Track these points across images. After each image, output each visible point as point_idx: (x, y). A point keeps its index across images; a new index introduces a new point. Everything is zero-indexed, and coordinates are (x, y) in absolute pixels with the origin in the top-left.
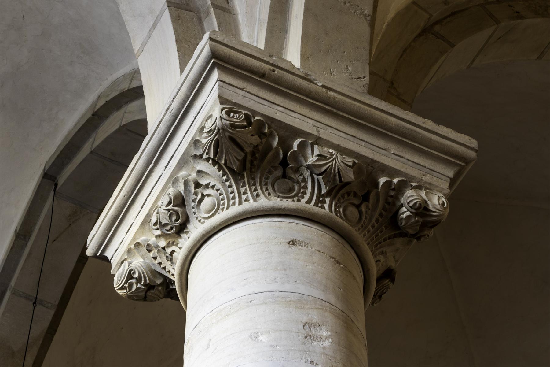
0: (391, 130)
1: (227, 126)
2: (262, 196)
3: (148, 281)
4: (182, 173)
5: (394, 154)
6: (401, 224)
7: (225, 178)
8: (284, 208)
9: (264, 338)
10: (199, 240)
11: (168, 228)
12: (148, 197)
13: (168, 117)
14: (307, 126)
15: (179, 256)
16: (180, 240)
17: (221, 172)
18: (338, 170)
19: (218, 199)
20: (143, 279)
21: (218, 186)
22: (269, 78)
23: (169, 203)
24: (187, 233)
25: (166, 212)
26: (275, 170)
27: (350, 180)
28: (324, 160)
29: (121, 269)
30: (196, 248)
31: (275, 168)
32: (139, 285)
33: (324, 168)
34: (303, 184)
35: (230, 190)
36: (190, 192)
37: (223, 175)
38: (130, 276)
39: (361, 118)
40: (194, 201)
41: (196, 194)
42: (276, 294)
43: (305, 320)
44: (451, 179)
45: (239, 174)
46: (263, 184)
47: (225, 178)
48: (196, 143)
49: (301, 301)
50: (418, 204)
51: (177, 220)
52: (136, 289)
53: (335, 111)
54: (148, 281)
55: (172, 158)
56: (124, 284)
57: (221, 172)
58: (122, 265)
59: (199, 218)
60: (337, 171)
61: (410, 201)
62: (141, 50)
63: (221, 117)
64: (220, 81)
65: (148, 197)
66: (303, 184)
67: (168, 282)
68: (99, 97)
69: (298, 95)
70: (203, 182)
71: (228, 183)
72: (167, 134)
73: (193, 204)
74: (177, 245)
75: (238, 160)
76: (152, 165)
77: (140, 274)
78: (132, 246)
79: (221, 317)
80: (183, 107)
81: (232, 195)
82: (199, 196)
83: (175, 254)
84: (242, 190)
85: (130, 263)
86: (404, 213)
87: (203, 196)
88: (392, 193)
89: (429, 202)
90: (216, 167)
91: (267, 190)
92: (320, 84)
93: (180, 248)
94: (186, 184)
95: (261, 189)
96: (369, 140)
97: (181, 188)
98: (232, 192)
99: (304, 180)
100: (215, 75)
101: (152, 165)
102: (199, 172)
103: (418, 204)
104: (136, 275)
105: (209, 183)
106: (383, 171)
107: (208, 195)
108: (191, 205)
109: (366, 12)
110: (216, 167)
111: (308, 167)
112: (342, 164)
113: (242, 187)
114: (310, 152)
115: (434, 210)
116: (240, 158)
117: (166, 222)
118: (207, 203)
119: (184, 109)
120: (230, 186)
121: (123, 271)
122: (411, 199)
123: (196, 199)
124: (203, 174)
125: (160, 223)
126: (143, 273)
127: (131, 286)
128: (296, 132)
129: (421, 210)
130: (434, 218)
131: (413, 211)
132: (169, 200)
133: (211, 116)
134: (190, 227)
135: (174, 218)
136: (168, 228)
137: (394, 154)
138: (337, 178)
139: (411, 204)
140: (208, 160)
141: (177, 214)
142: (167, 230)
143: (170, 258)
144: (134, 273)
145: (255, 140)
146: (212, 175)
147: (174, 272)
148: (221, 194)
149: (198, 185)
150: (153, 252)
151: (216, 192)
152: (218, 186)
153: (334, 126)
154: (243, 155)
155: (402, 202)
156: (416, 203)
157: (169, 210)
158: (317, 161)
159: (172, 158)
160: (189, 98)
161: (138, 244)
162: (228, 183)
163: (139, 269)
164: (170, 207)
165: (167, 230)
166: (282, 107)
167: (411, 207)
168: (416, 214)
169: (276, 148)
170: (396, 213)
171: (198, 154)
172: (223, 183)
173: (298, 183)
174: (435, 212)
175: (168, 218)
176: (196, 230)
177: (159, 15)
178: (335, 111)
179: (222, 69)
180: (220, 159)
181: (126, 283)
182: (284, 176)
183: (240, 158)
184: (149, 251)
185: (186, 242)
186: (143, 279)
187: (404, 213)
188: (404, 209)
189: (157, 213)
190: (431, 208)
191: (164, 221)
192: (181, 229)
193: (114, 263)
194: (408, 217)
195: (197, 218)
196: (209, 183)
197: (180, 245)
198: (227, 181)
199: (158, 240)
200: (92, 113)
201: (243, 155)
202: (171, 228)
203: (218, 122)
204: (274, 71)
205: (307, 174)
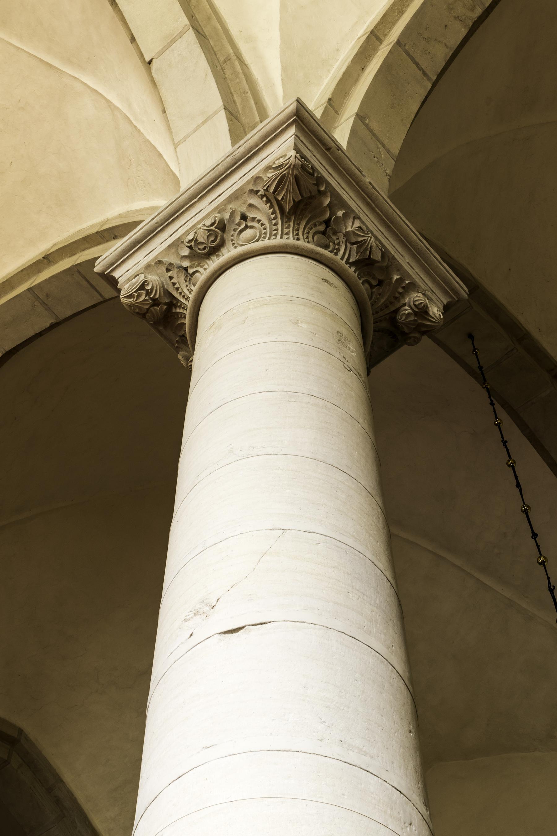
0: (410, 242)
1: (298, 165)
2: (302, 240)
3: (157, 296)
4: (232, 206)
5: (408, 263)
6: (401, 319)
7: (273, 216)
8: (322, 254)
9: (304, 326)
10: (234, 259)
11: (202, 247)
12: (181, 227)
13: (229, 160)
14: (353, 205)
15: (202, 276)
16: (208, 262)
17: (271, 210)
18: (371, 248)
19: (260, 232)
20: (154, 293)
21: (265, 221)
22: (332, 154)
23: (212, 224)
24: (218, 256)
25: (206, 232)
26: (320, 225)
27: (377, 259)
28: (362, 233)
29: (134, 280)
30: (228, 266)
31: (321, 224)
32: (147, 298)
33: (361, 239)
34: (337, 247)
35: (274, 227)
36: (233, 222)
37: (272, 214)
38: (142, 287)
39: (392, 222)
40: (235, 230)
41: (239, 224)
42: (313, 303)
43: (338, 329)
44: (444, 305)
45: (287, 217)
46: (305, 232)
47: (273, 216)
48: (257, 179)
49: (334, 316)
50: (423, 305)
51: (213, 241)
52: (144, 301)
53: (374, 206)
54: (157, 296)
55: (220, 195)
56: (134, 292)
57: (271, 210)
58: (136, 278)
59: (236, 245)
60: (369, 247)
61: (417, 300)
62: (182, 141)
63: (296, 156)
64: (296, 135)
65: (181, 227)
66: (337, 247)
67: (173, 303)
68: (54, 245)
69: (350, 179)
70: (250, 215)
71: (274, 222)
72: (222, 174)
73: (233, 232)
74: (201, 267)
75: (294, 200)
76: (196, 200)
77: (152, 289)
78: (153, 264)
79: (259, 305)
80: (248, 154)
81: (274, 232)
82: (243, 226)
83: (197, 274)
84: (286, 231)
85: (145, 277)
86: (406, 310)
87: (247, 227)
88: (400, 290)
89: (430, 308)
90: (268, 205)
91: (307, 237)
92: (368, 181)
93: (205, 269)
94: (232, 214)
95: (303, 235)
96: (392, 243)
97: (227, 216)
98: (275, 230)
99: (339, 244)
100: (293, 130)
101: (196, 200)
102: (251, 205)
103: (423, 305)
104: (149, 287)
105: (256, 218)
106: (398, 270)
107: (252, 227)
108: (230, 233)
109: (387, 172)
110: (268, 205)
111: (347, 235)
112: (374, 243)
113: (286, 228)
114: (350, 223)
115: (433, 316)
116: (296, 200)
117: (202, 240)
118: (248, 233)
119: (249, 155)
120: (276, 224)
121: (135, 283)
122: (418, 298)
123: (237, 229)
124: (253, 209)
125: (196, 240)
126: (156, 287)
127: (139, 296)
128: (343, 204)
129: (422, 311)
130: (430, 323)
131: (416, 310)
132: (213, 221)
133: (285, 156)
134: (224, 250)
135: (212, 239)
136: (202, 247)
137: (408, 263)
138: (368, 252)
139: (417, 303)
140: (262, 197)
141: (216, 237)
142: (199, 249)
143: (189, 277)
144: (148, 284)
145: (314, 189)
146: (262, 211)
147: (188, 293)
148: (265, 229)
149: (244, 217)
150: (171, 272)
151: (260, 226)
152: (265, 221)
153: (370, 217)
154: (300, 198)
155: (407, 301)
156: (421, 303)
157: (209, 231)
158: (357, 230)
159: (220, 195)
160: (257, 146)
161: (160, 262)
162: (274, 222)
163: (154, 282)
164: (213, 228)
165: (199, 249)
166: (336, 181)
167: (415, 305)
168: (416, 314)
169: (325, 207)
170: (397, 311)
171: (255, 189)
172: (270, 220)
173: (334, 243)
174: (433, 318)
175: (206, 238)
176: (228, 253)
177: (212, 115)
178: (374, 206)
179: (299, 128)
180: (278, 194)
181: (136, 292)
182: (324, 233)
183: (296, 200)
184: (168, 270)
185: (214, 264)
186: (154, 293)
187: (406, 310)
188: (407, 307)
189: (195, 233)
190: (431, 313)
191: (200, 240)
192: (214, 251)
193: (121, 281)
194: (409, 314)
195: (233, 244)
196: (256, 218)
197: (206, 266)
198: (274, 219)
199: (182, 261)
200: (43, 256)
201: (300, 198)
202: (205, 248)
203: (292, 159)
204: (194, 285)
205: (342, 240)
